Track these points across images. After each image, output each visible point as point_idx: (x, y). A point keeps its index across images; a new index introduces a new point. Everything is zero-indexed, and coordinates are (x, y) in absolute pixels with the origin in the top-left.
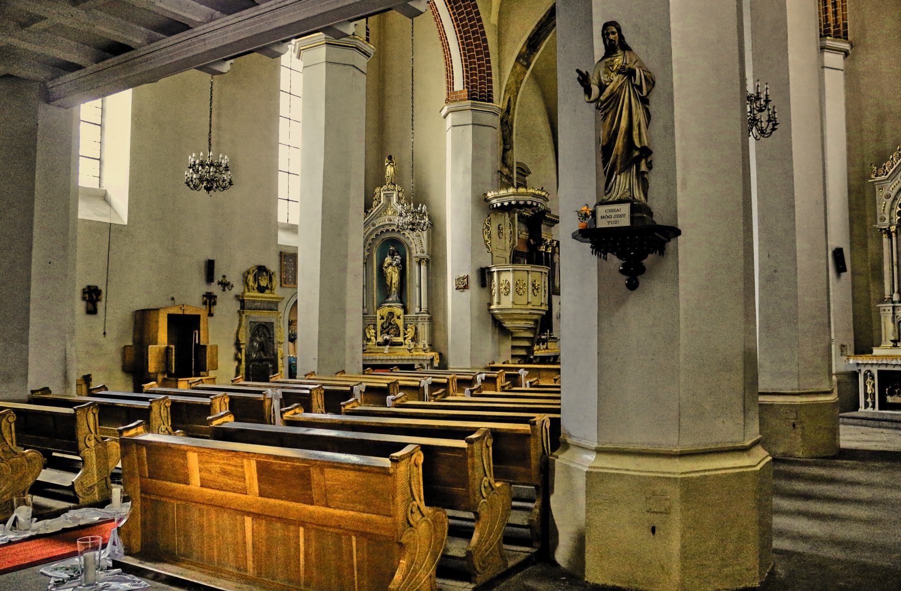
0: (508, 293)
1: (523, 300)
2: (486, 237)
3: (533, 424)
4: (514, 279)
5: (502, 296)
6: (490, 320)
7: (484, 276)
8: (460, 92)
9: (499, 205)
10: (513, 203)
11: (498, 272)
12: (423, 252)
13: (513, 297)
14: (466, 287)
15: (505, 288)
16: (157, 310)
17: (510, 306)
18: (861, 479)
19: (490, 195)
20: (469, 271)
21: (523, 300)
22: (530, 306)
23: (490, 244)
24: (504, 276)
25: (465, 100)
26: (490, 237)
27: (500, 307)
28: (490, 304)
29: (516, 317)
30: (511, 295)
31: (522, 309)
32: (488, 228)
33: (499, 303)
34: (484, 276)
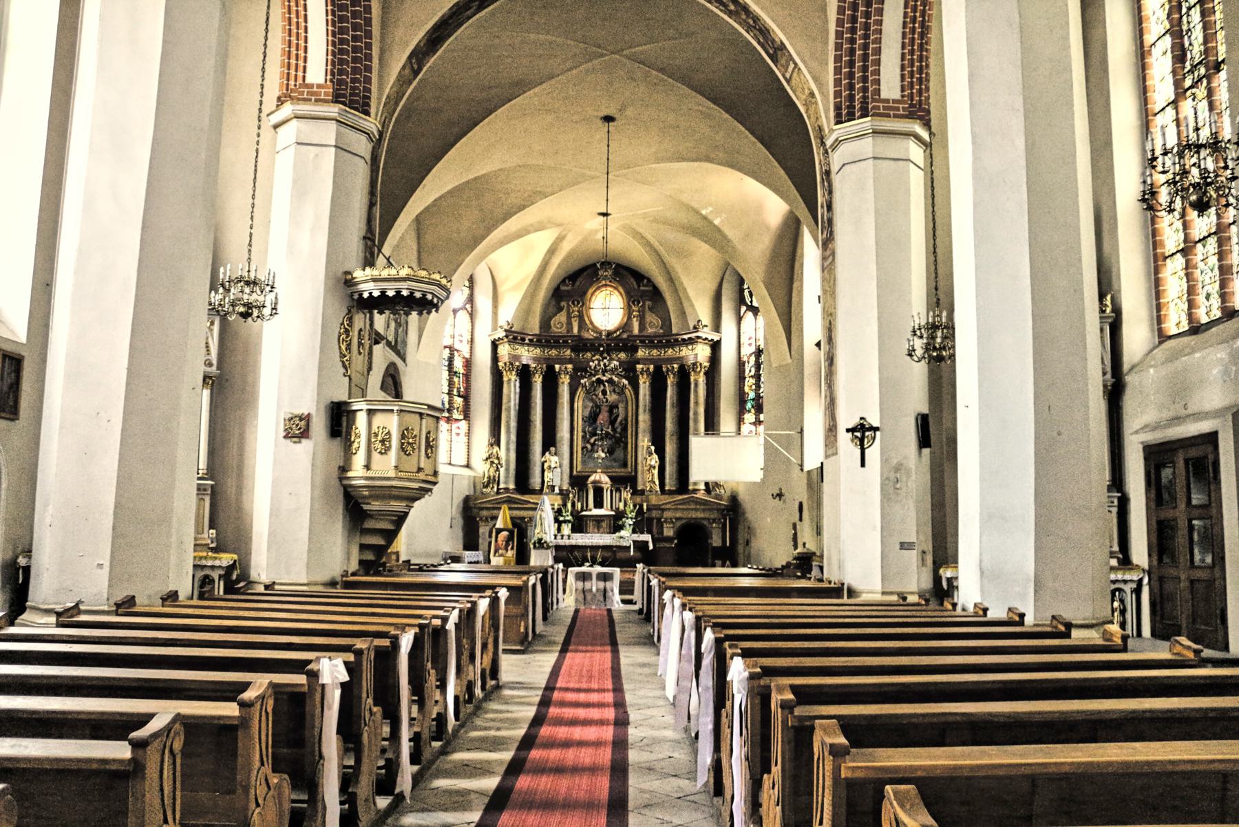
0: (388, 449)
1: (411, 464)
2: (343, 347)
3: (313, 675)
4: (400, 425)
5: (375, 455)
6: (341, 497)
7: (339, 419)
8: (319, 86)
9: (376, 294)
10: (405, 293)
11: (371, 412)
12: (210, 365)
13: (399, 459)
14: (305, 434)
15: (383, 441)
16: (345, 488)
17: (392, 474)
18: (709, 761)
19: (359, 274)
20: (309, 403)
21: (411, 464)
22: (421, 476)
23: (349, 360)
24: (378, 420)
25: (326, 101)
26: (349, 347)
27: (370, 474)
28: (344, 469)
29: (395, 492)
30: (393, 453)
31: (409, 480)
32: (347, 331)
33: (368, 467)
34: (339, 419)
